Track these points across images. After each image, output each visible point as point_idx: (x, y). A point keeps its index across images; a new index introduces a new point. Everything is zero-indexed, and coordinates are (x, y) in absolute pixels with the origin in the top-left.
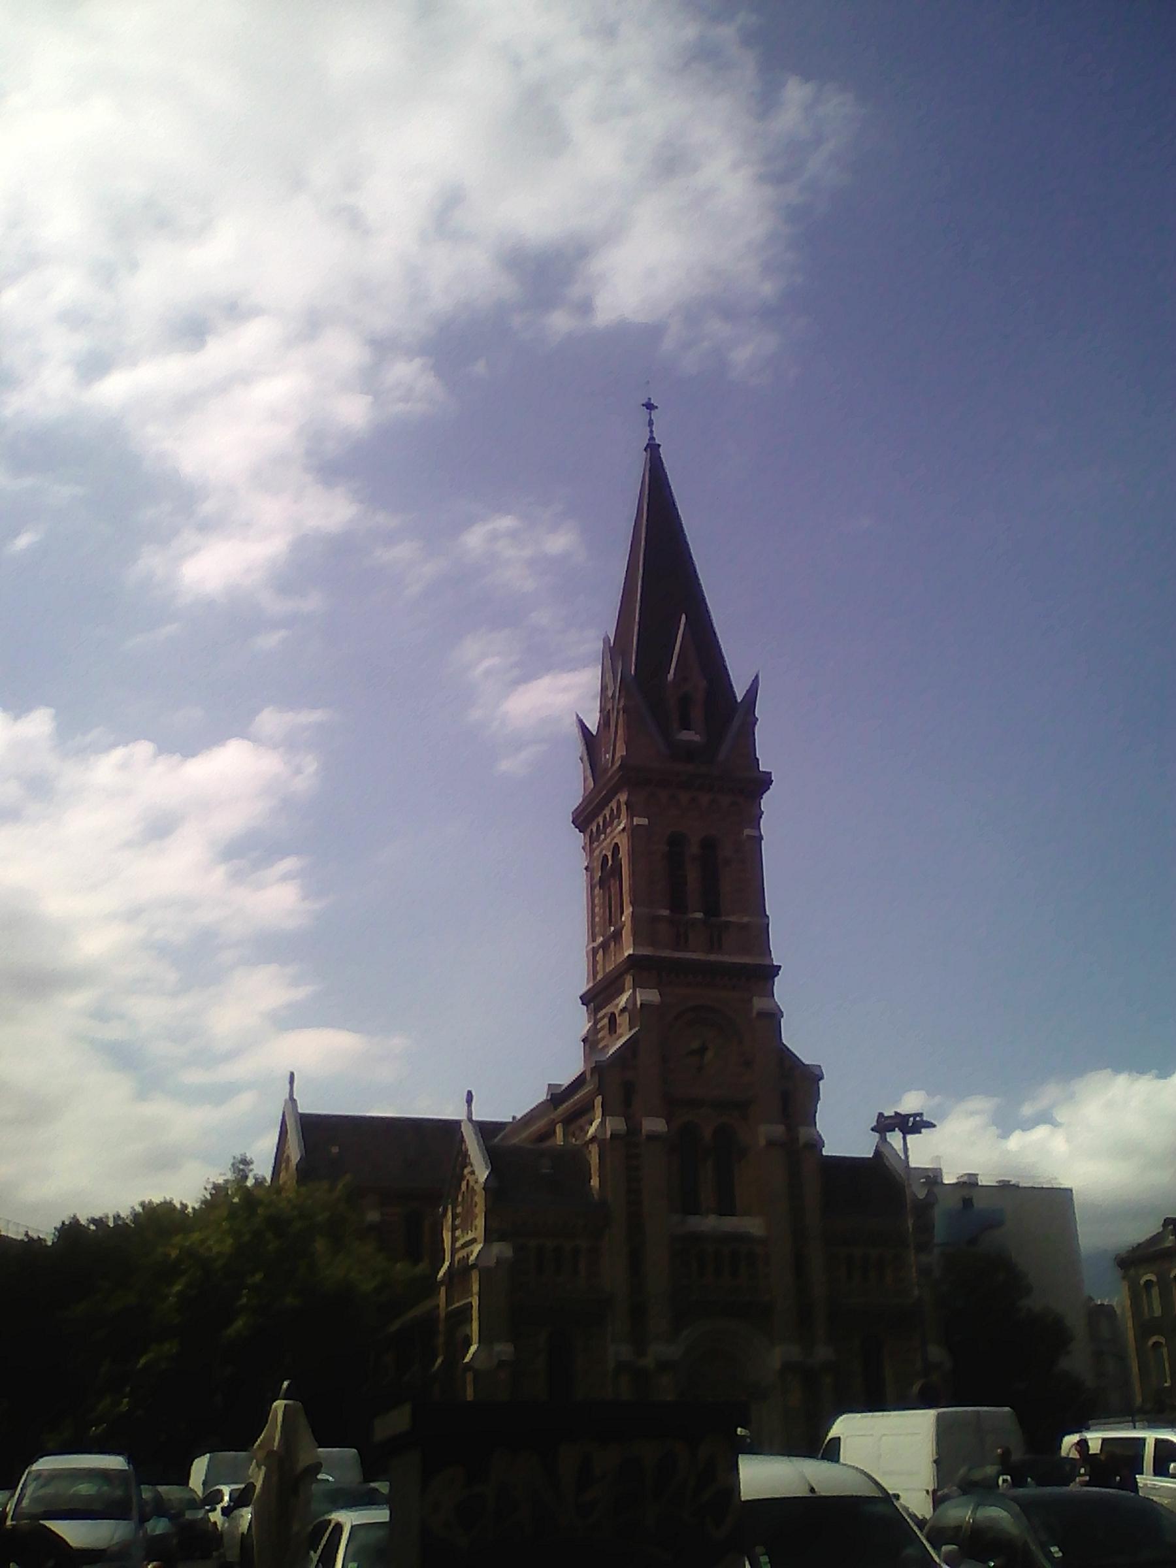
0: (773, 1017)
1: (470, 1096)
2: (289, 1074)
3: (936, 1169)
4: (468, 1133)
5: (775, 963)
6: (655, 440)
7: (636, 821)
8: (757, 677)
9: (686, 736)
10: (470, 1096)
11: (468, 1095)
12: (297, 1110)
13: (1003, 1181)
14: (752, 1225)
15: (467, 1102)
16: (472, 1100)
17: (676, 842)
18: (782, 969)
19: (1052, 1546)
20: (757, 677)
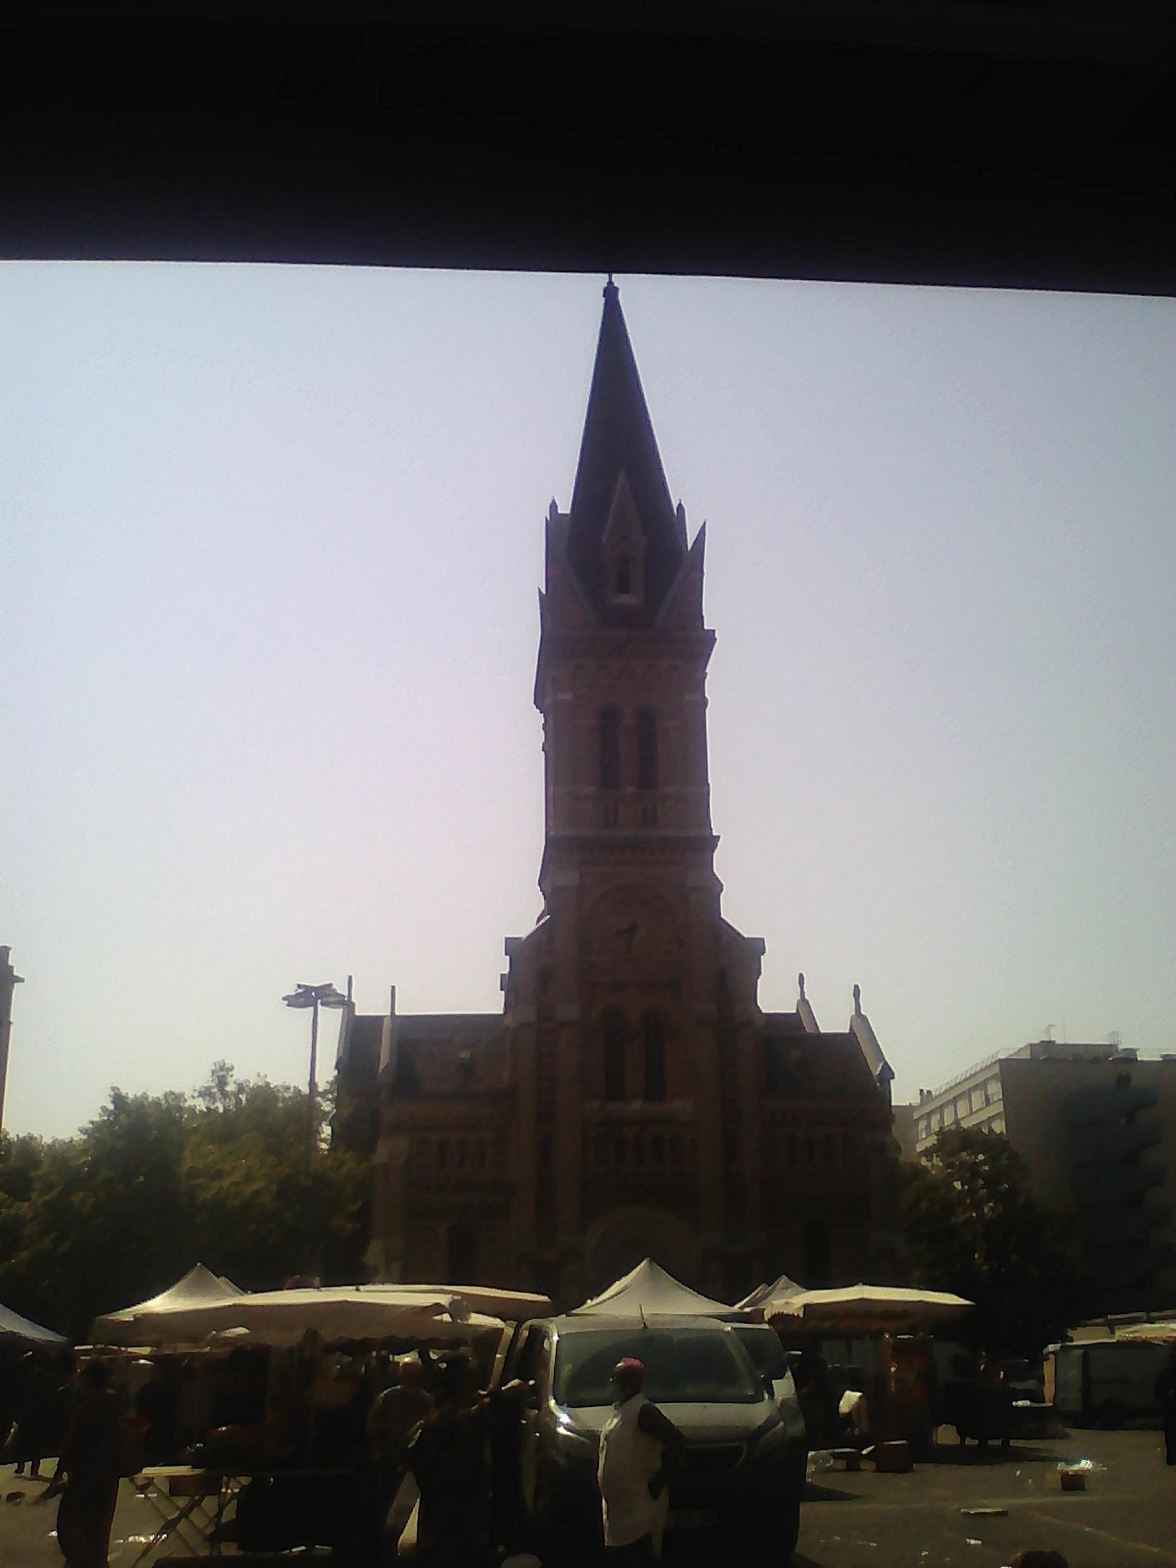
0: (713, 889)
1: (857, 990)
2: (347, 979)
3: (1111, 1045)
4: (387, 1024)
5: (714, 833)
6: (613, 283)
7: (561, 697)
8: (704, 524)
9: (624, 599)
10: (857, 990)
11: (855, 990)
12: (354, 1012)
13: (1167, 1055)
14: (679, 1107)
15: (854, 996)
16: (859, 995)
17: (608, 718)
18: (721, 840)
19: (519, 1384)
20: (704, 524)
